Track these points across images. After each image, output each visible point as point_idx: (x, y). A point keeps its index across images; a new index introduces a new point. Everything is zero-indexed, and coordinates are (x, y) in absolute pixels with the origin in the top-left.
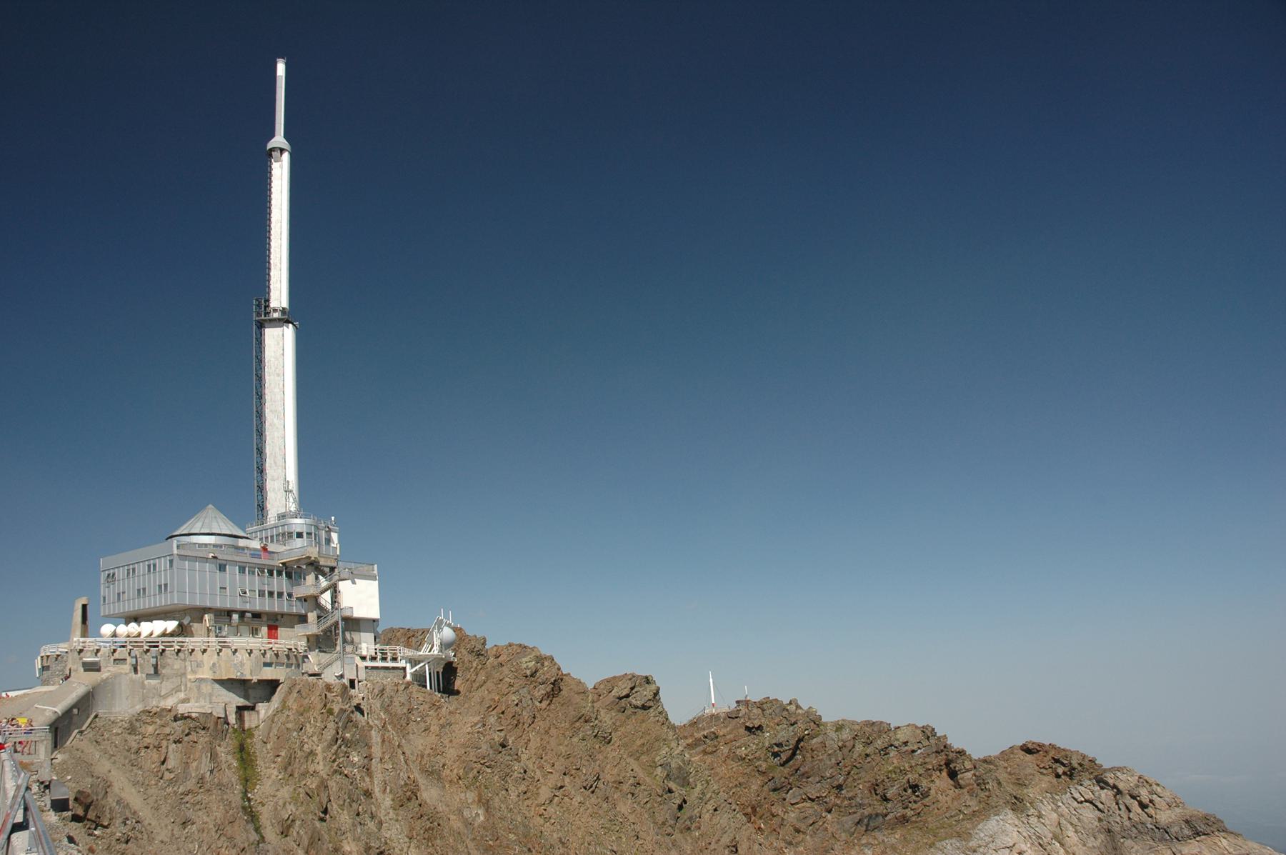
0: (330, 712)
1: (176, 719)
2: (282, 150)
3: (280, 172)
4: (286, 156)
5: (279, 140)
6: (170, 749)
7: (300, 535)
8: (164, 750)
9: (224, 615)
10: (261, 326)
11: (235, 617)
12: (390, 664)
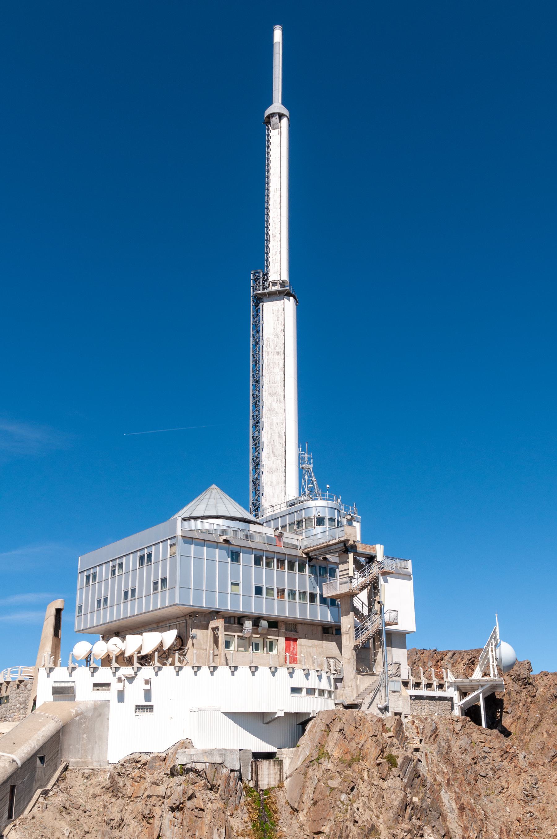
0: (392, 761)
1: (173, 773)
2: (281, 116)
3: (278, 140)
4: (285, 122)
6: (166, 822)
7: (320, 521)
8: (156, 823)
9: (235, 621)
10: (259, 300)
11: (248, 624)
12: (437, 693)
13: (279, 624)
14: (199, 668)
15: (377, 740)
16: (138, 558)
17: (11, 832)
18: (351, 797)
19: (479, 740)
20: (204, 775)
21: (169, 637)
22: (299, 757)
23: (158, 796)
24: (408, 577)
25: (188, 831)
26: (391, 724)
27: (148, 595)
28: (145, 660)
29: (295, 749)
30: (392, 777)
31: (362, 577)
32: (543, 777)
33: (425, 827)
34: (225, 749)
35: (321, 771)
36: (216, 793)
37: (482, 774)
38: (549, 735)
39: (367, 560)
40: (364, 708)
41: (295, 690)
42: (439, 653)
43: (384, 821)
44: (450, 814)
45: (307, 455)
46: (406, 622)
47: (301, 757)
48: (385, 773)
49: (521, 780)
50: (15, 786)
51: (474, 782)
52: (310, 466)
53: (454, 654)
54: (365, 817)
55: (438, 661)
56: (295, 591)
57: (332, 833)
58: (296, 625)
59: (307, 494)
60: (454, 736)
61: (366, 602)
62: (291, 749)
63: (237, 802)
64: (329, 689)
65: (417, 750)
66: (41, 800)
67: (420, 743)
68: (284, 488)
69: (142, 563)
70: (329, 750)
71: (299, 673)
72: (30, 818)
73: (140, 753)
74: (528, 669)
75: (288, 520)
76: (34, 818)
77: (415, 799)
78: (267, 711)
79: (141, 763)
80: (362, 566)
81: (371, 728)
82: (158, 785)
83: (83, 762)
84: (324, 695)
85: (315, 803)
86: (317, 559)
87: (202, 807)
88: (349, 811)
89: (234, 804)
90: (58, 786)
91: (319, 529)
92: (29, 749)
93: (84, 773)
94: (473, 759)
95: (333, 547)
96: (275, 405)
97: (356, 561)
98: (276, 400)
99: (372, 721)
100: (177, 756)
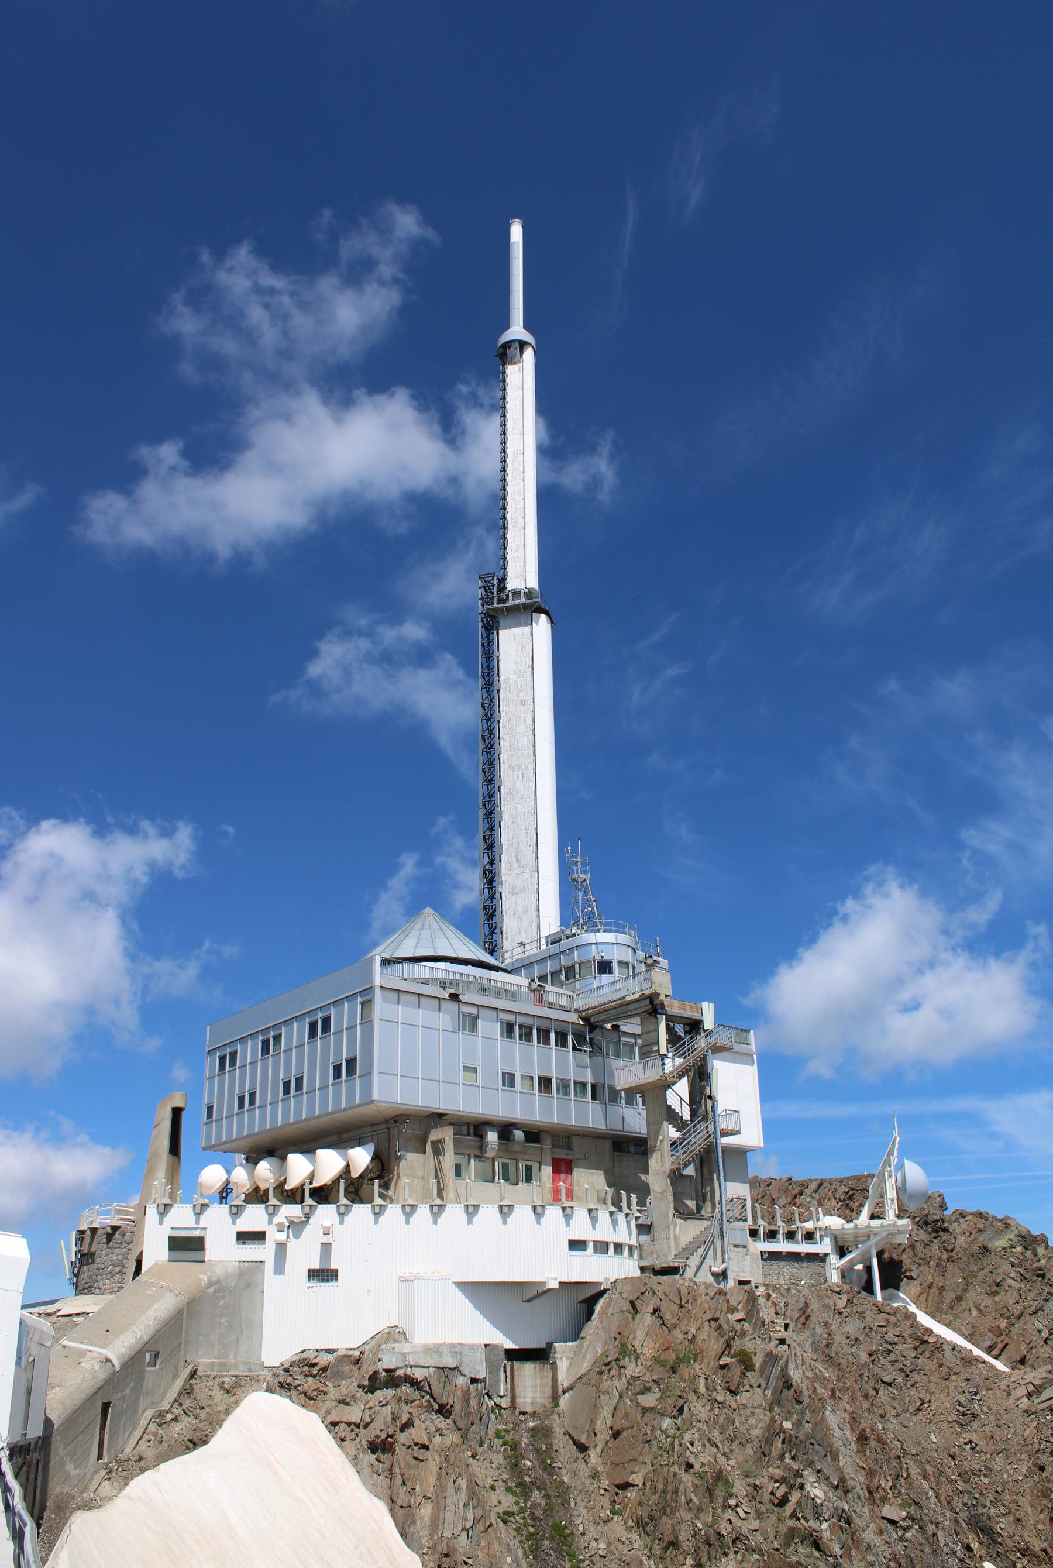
0: (746, 1361)
1: (373, 1384)
4: (529, 354)
5: (517, 330)
9: (473, 1129)
11: (492, 1137)
12: (803, 1248)
13: (543, 1136)
14: (413, 1207)
15: (720, 1326)
16: (307, 1026)
17: (103, 1484)
18: (679, 1422)
19: (877, 1324)
20: (427, 1389)
21: (361, 1157)
22: (584, 1357)
23: (349, 1424)
24: (750, 1058)
25: (404, 1483)
26: (737, 1298)
27: (324, 1088)
28: (323, 1195)
29: (576, 1343)
30: (747, 1387)
31: (679, 1057)
32: (988, 1382)
33: (805, 1473)
34: (461, 1344)
35: (624, 1380)
36: (448, 1418)
37: (887, 1379)
38: (980, 1311)
39: (687, 1029)
40: (689, 1273)
41: (576, 1245)
42: (795, 1182)
43: (737, 1463)
44: (843, 1449)
45: (579, 859)
46: (750, 1134)
47: (588, 1357)
48: (735, 1382)
49: (952, 1388)
50: (110, 1403)
51: (874, 1393)
52: (585, 876)
53: (821, 1184)
54: (702, 1457)
55: (795, 1197)
56: (569, 1080)
57: (648, 1484)
58: (569, 1137)
59: (581, 921)
60: (837, 1316)
61: (686, 1098)
62: (570, 1344)
63: (483, 1434)
64: (631, 1243)
65: (782, 1341)
66: (153, 1427)
67: (786, 1329)
68: (535, 920)
69: (313, 1033)
70: (637, 1344)
71: (580, 1215)
72: (134, 1459)
73: (317, 1350)
74: (941, 1207)
75: (549, 966)
76: (141, 1459)
77: (787, 1425)
78: (533, 1280)
79: (318, 1368)
80: (680, 1038)
81: (706, 1306)
82: (348, 1404)
83: (220, 1364)
84: (622, 1253)
85: (616, 1435)
86: (602, 1028)
87: (426, 1442)
88: (676, 1447)
89: (478, 1437)
90: (181, 1405)
91: (606, 978)
92: (133, 1340)
93: (223, 1382)
94: (870, 1355)
95: (630, 1007)
96: (519, 784)
97: (669, 1030)
98: (520, 776)
99: (707, 1294)
100: (380, 1356)
